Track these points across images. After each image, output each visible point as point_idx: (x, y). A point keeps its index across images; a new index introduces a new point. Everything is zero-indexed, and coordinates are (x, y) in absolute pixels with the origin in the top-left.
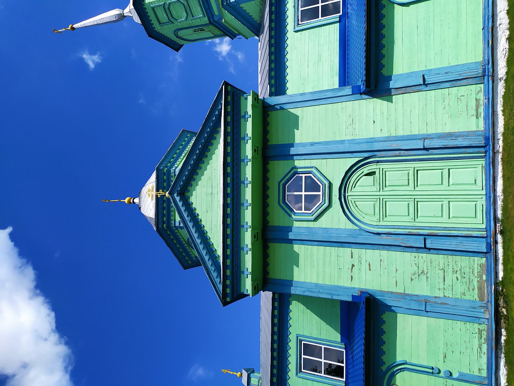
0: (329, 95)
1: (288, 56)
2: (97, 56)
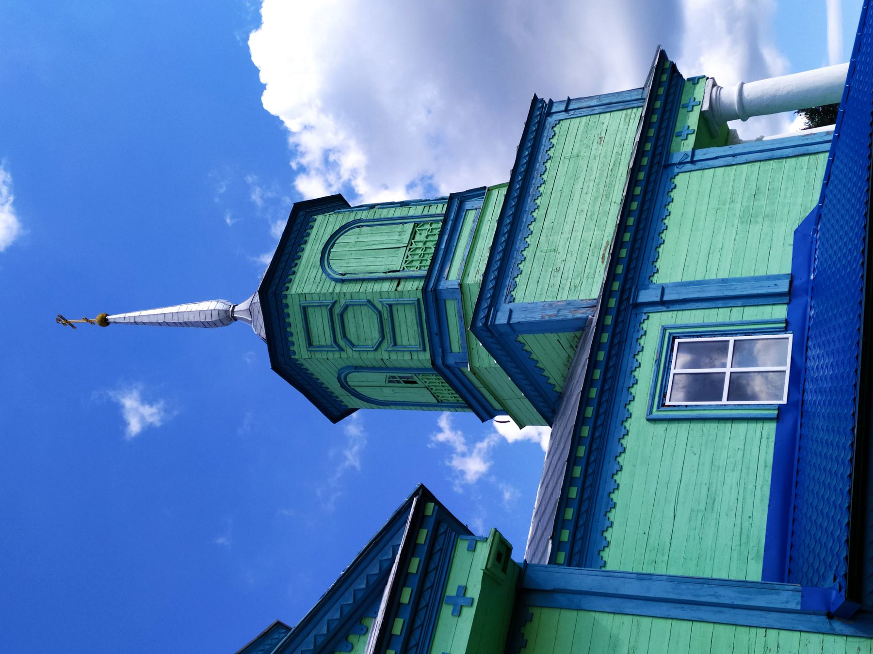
0: (728, 596)
1: (621, 478)
2: (154, 410)
